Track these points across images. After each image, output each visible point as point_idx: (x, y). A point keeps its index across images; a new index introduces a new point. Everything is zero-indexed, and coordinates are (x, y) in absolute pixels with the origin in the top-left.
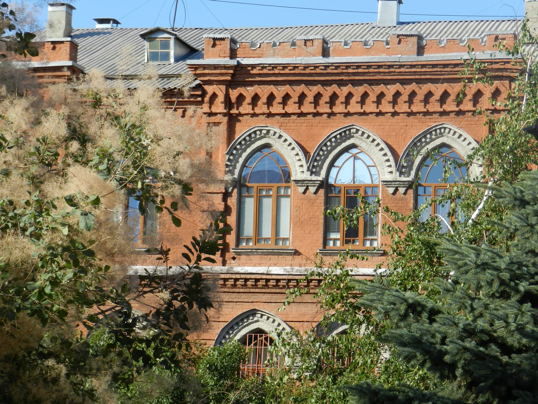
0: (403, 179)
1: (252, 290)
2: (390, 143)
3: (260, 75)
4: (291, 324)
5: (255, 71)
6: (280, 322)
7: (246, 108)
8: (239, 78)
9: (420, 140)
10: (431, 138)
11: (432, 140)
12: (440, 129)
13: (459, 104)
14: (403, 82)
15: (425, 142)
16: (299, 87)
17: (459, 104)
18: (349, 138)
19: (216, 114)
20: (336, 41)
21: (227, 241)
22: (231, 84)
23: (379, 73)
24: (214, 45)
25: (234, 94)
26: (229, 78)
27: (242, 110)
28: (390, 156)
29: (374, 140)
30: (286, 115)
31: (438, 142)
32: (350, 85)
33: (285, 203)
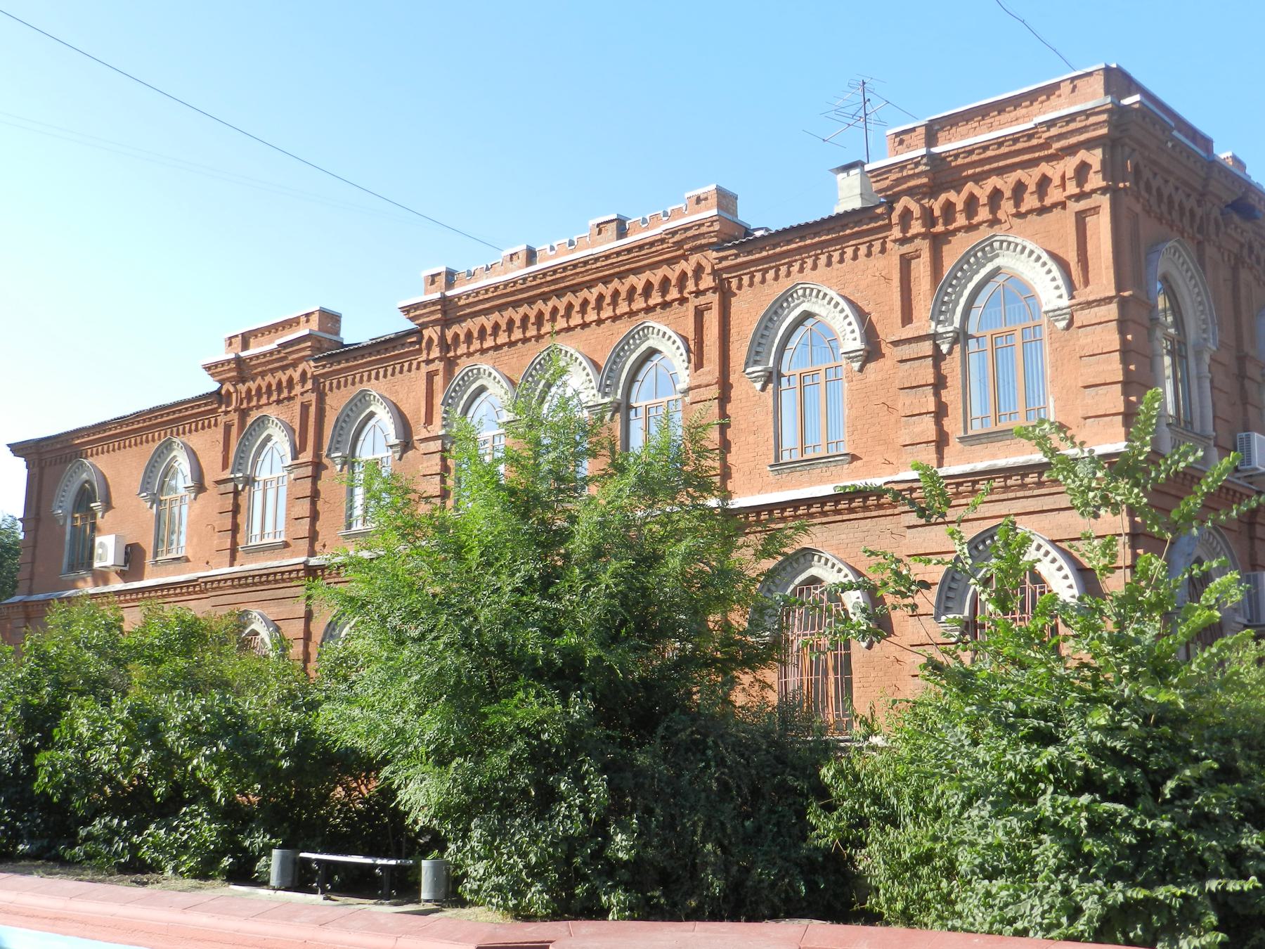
0: (607, 400)
1: (1036, 492)
2: (1056, 251)
3: (468, 305)
4: (1065, 545)
5: (462, 302)
6: (1042, 542)
7: (462, 349)
8: (451, 315)
9: (623, 349)
10: (634, 343)
11: (637, 346)
12: (643, 329)
13: (664, 294)
14: (606, 280)
15: (630, 349)
16: (1036, 169)
17: (664, 294)
18: (991, 260)
19: (433, 361)
20: (633, 218)
21: (945, 428)
22: (933, 190)
23: (577, 274)
24: (600, 232)
25: (449, 334)
26: (1104, 131)
27: (459, 352)
28: (1056, 272)
29: (1032, 252)
30: (497, 348)
31: (643, 347)
32: (665, 267)
33: (973, 360)
